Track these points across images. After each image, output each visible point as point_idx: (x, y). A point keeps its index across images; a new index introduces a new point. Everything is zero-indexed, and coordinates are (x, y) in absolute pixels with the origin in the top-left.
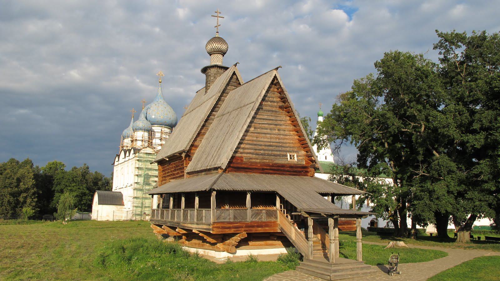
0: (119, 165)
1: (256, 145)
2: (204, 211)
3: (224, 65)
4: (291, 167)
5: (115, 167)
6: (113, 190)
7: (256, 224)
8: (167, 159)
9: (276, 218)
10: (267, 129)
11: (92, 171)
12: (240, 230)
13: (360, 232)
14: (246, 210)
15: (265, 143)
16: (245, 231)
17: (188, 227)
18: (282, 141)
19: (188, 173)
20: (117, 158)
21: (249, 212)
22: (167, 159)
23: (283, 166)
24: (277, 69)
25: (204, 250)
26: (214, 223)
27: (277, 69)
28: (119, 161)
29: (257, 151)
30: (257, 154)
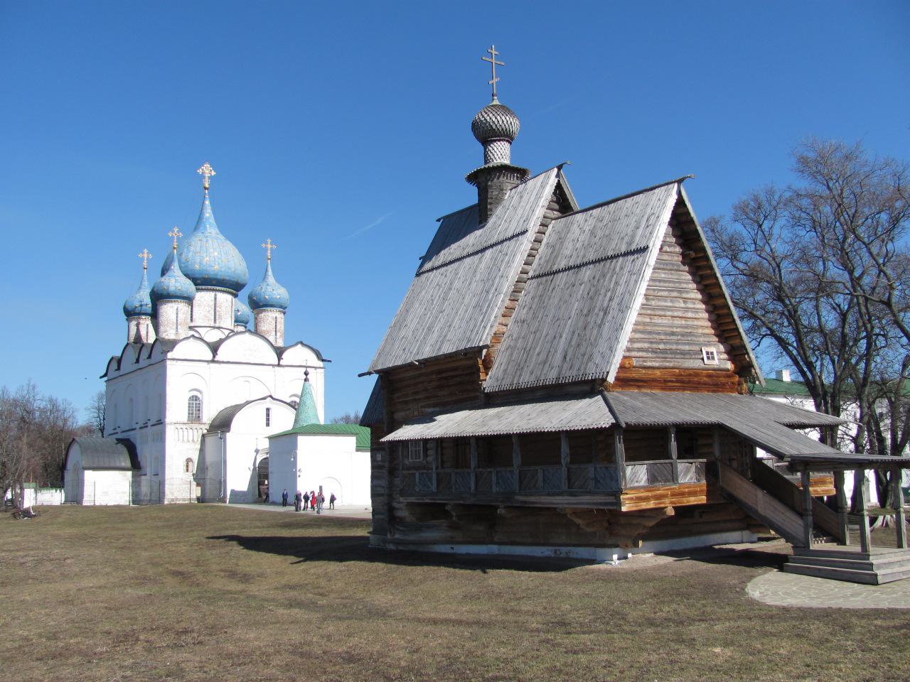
1: (650, 333)
7: (687, 490)
8: (417, 363)
12: (663, 503)
13: (694, 501)
15: (664, 329)
17: (533, 503)
18: (690, 323)
22: (417, 363)
23: (696, 373)
25: (557, 548)
28: (119, 369)
29: (654, 346)
30: (654, 351)
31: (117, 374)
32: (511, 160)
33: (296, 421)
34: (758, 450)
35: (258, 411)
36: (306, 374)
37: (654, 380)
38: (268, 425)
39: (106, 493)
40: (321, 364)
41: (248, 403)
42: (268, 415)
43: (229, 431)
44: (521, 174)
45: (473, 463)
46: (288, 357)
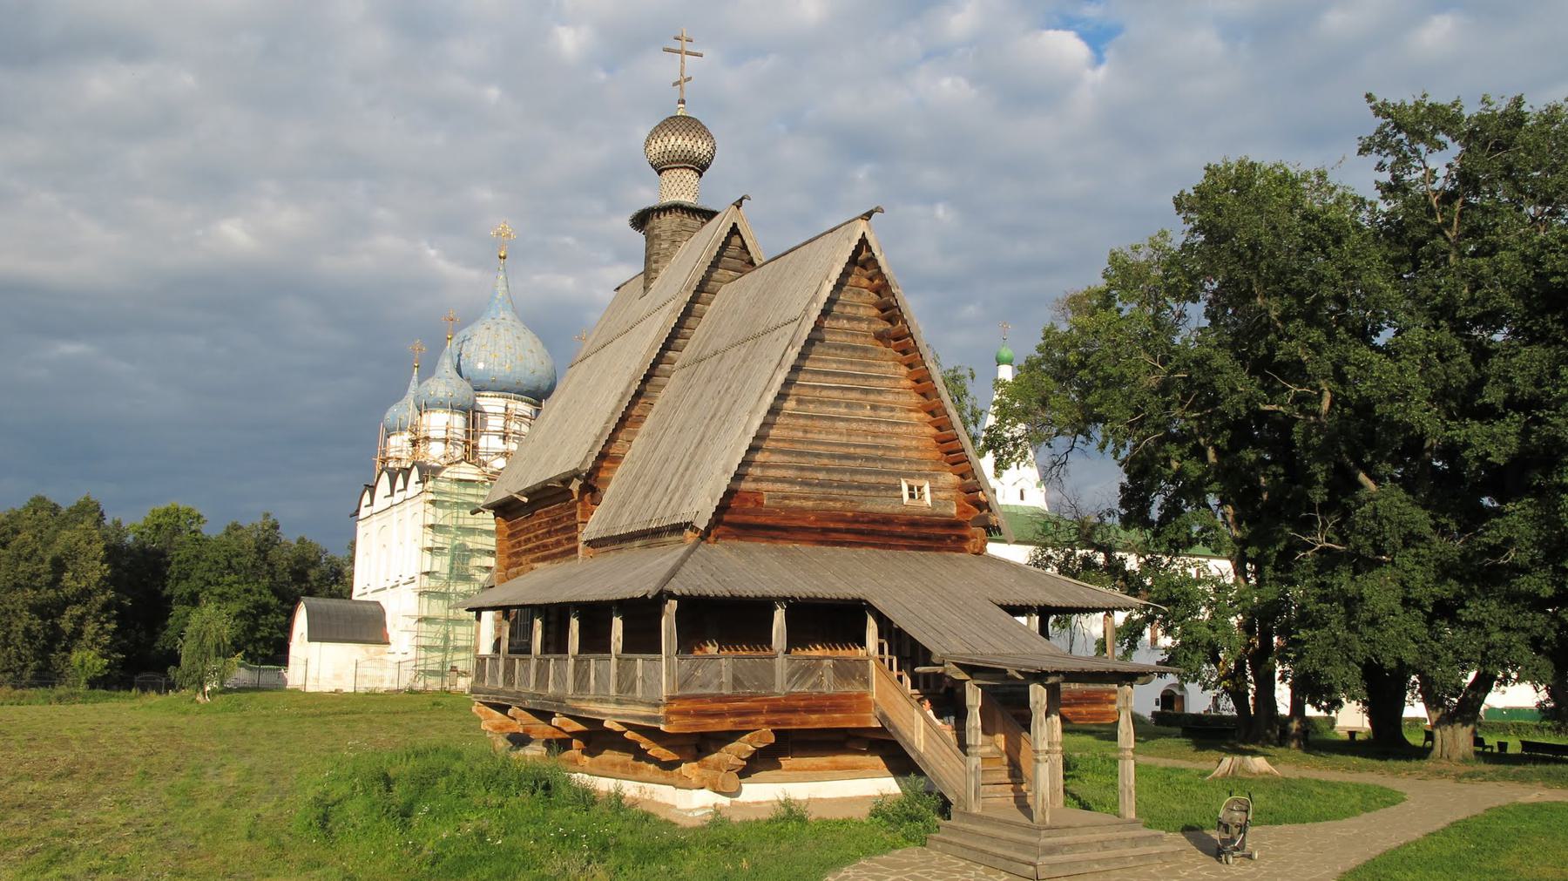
2: (639, 662)
4: (913, 523)
6: (355, 597)
9: (867, 682)
10: (836, 404)
11: (289, 536)
16: (768, 723)
19: (590, 543)
23: (887, 520)
26: (671, 699)
28: (372, 504)
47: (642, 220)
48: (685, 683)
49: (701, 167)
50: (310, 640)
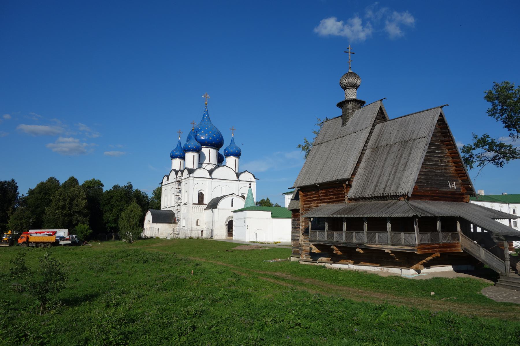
0: (169, 185)
2: (317, 232)
3: (359, 99)
4: (452, 194)
5: (163, 187)
6: (161, 209)
9: (458, 240)
10: (433, 161)
11: (134, 188)
14: (438, 233)
16: (439, 251)
19: (349, 199)
20: (166, 178)
21: (441, 235)
23: (446, 193)
24: (381, 100)
26: (419, 245)
27: (381, 100)
28: (168, 180)
31: (167, 183)
32: (357, 97)
33: (245, 205)
34: (477, 227)
35: (228, 200)
36: (250, 184)
37: (428, 196)
38: (232, 206)
39: (162, 234)
40: (255, 180)
41: (224, 196)
42: (232, 202)
43: (42, 183)
44: (360, 103)
45: (326, 228)
46: (241, 177)
47: (341, 105)
48: (421, 241)
49: (356, 87)
50: (153, 222)
